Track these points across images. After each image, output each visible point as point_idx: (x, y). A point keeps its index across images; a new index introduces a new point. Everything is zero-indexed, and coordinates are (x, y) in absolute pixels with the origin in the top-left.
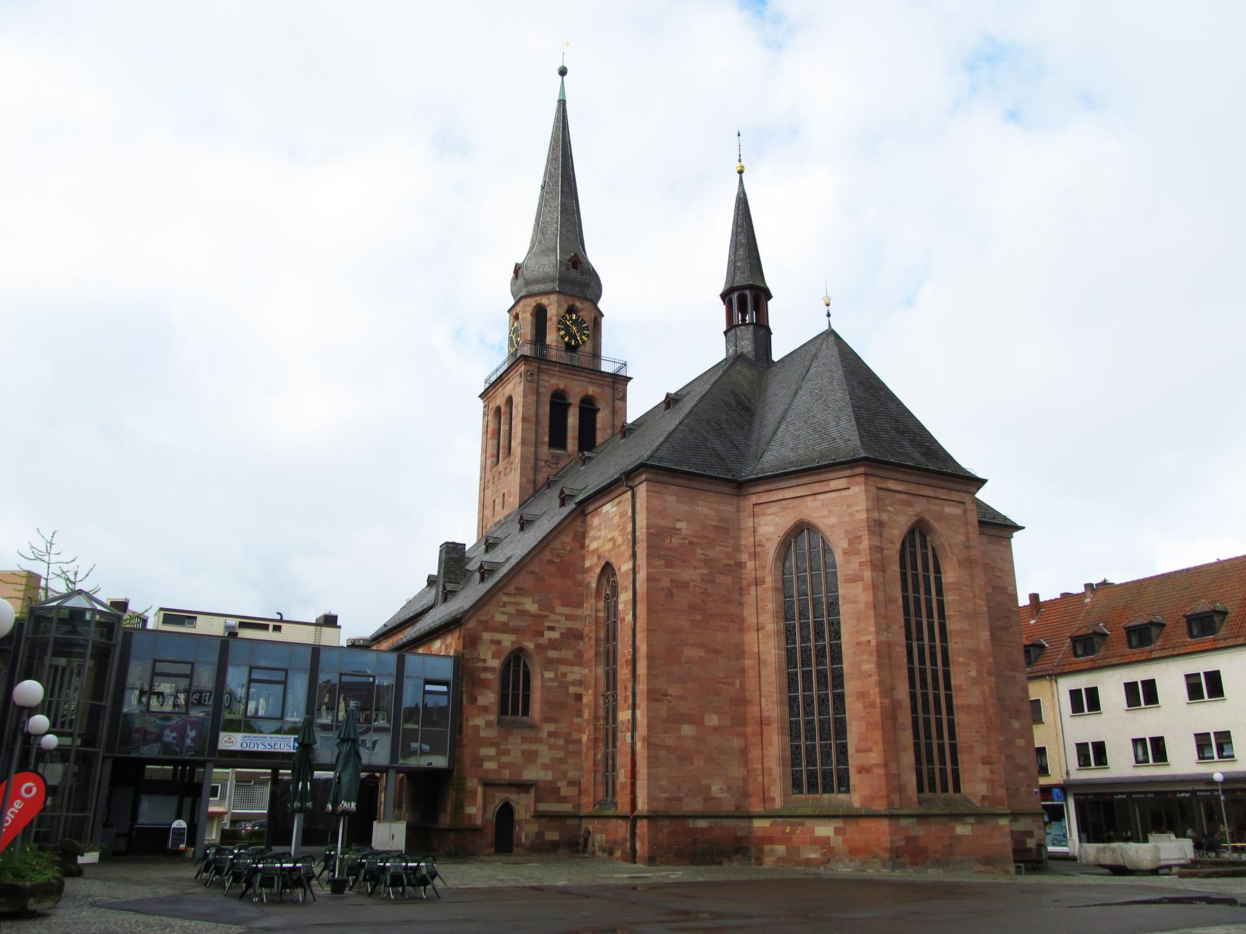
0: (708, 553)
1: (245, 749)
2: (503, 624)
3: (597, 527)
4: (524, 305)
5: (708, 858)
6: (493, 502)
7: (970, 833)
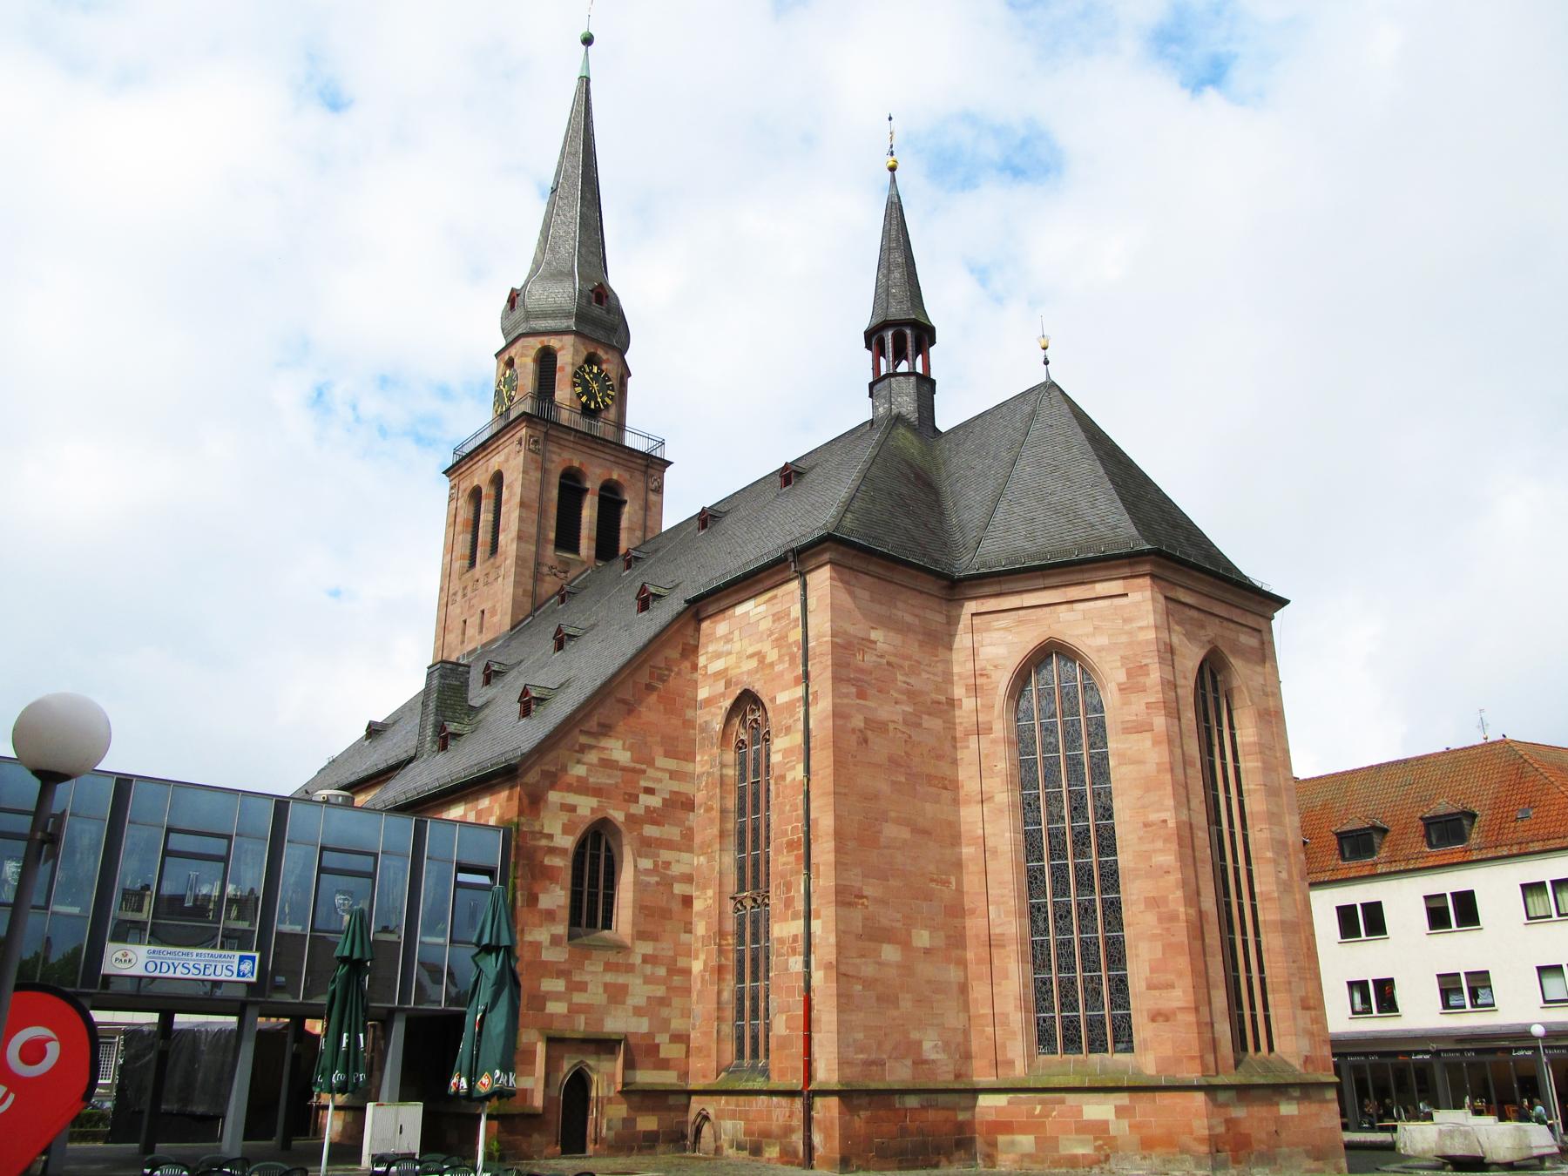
0: (911, 681)
1: (151, 975)
3: (725, 636)
4: (523, 347)
5: (920, 1158)
6: (462, 624)
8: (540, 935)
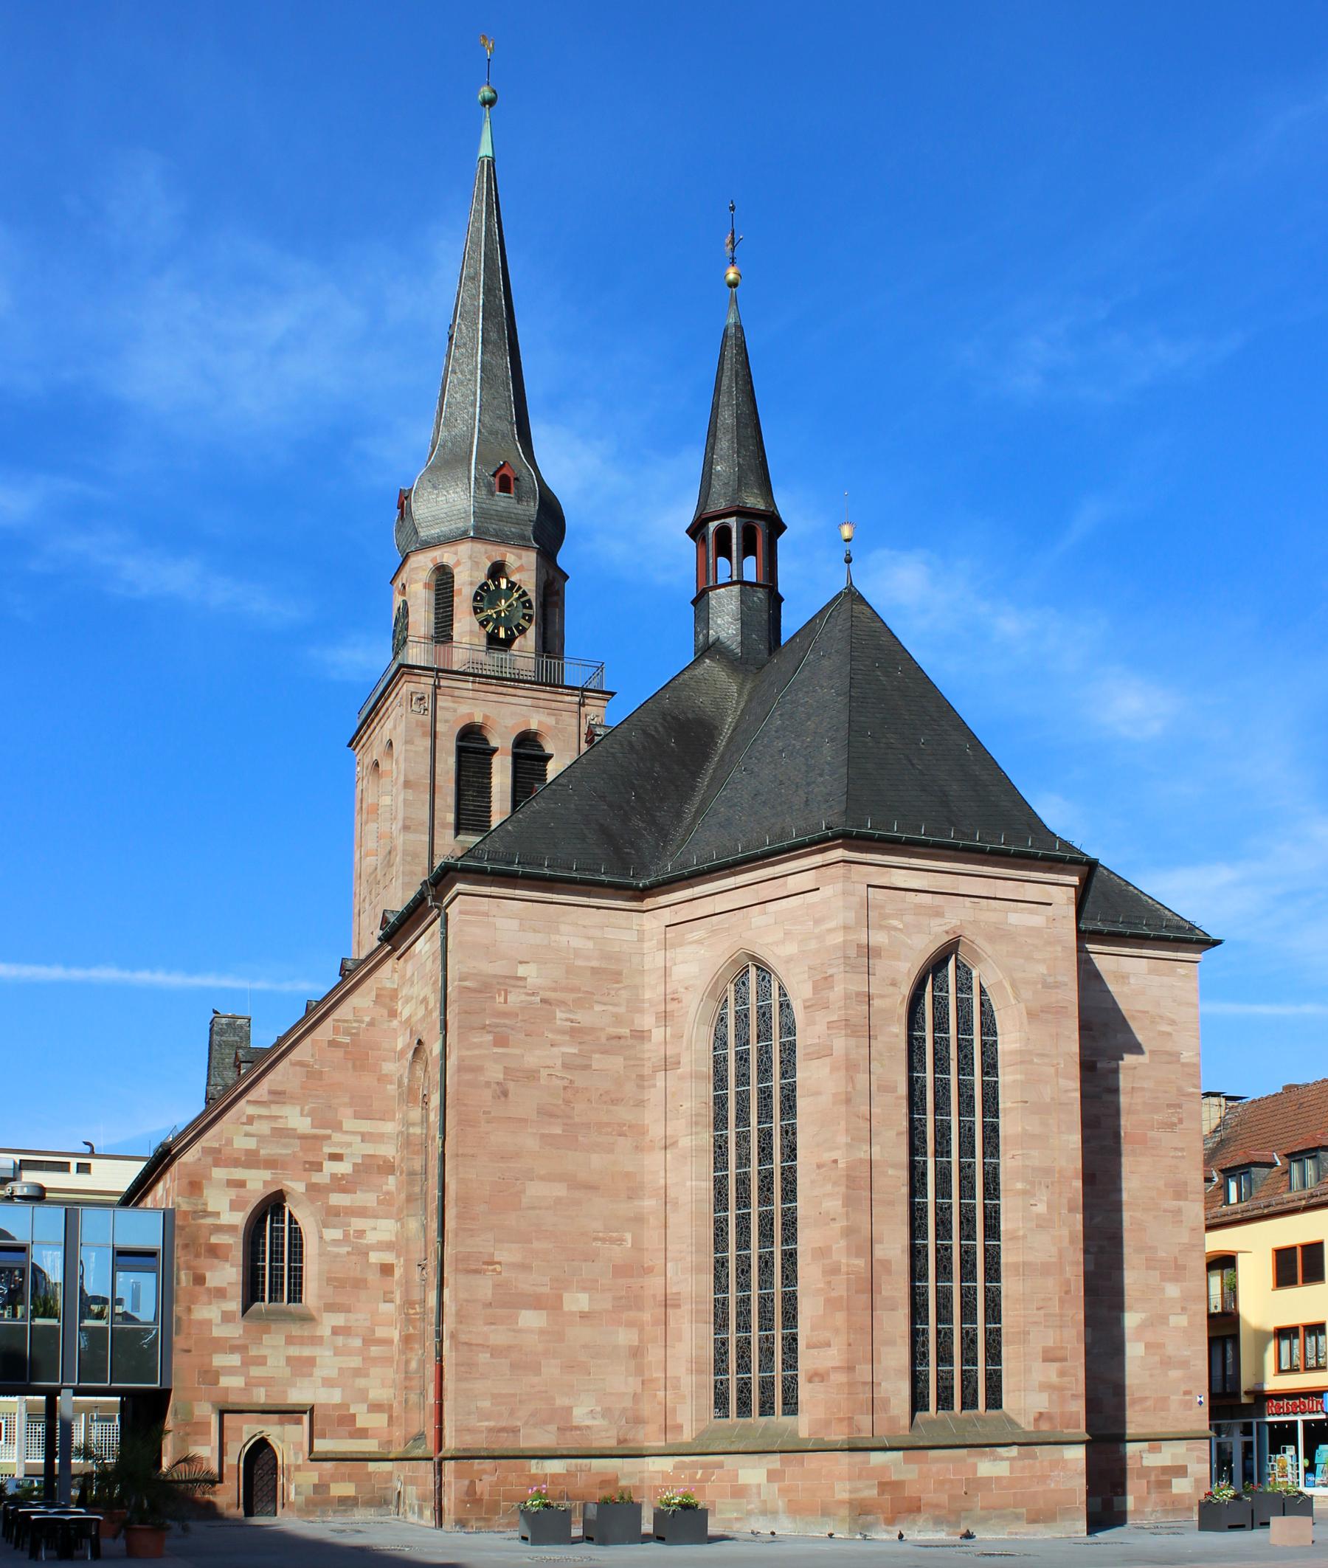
0: (578, 1017)
2: (248, 1152)
7: (1007, 1474)
8: (208, 1312)
